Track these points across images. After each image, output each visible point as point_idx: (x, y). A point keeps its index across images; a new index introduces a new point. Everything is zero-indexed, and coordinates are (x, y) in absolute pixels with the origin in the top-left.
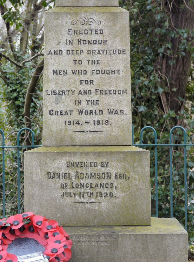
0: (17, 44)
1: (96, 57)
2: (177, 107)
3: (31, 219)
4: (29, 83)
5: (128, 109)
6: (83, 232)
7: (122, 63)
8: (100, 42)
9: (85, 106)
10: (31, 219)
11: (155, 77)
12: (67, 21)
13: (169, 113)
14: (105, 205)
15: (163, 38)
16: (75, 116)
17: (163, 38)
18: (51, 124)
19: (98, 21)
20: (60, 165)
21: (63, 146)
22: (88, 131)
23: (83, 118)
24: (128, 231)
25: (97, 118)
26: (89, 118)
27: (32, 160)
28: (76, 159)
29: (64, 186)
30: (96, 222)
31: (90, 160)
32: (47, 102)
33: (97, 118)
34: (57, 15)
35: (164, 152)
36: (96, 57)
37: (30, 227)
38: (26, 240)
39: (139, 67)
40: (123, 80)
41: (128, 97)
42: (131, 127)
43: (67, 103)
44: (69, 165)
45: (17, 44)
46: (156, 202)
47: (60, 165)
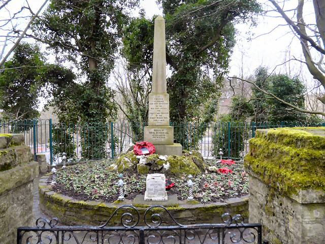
0: (144, 100)
1: (161, 105)
2: (182, 117)
3: (145, 143)
4: (146, 111)
5: (169, 118)
6: (158, 146)
7: (167, 106)
8: (162, 101)
9: (158, 116)
10: (145, 143)
11: (177, 110)
12: (154, 96)
13: (180, 119)
14: (163, 140)
15: (179, 100)
16: (156, 119)
17: (179, 100)
18: (151, 121)
19: (162, 96)
20: (152, 130)
21: (153, 126)
22: (159, 122)
23: (158, 119)
24: (168, 146)
25: (161, 119)
26: (160, 119)
27: (146, 128)
28: (156, 129)
29: (153, 135)
30: (316, 205)
31: (160, 129)
32: (150, 116)
33: (161, 119)
34: (152, 95)
35: (179, 128)
36: (161, 105)
37: (145, 145)
38: (144, 148)
39: (171, 105)
40: (168, 111)
41: (169, 115)
42: (169, 122)
43: (154, 116)
44: (155, 130)
45: (144, 102)
46: (114, 116)
47: (152, 130)
